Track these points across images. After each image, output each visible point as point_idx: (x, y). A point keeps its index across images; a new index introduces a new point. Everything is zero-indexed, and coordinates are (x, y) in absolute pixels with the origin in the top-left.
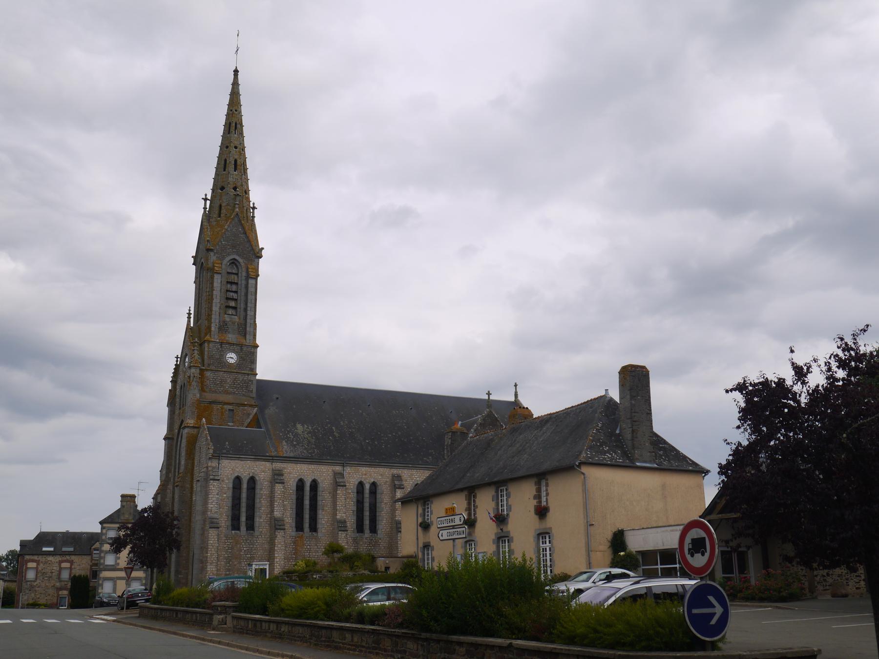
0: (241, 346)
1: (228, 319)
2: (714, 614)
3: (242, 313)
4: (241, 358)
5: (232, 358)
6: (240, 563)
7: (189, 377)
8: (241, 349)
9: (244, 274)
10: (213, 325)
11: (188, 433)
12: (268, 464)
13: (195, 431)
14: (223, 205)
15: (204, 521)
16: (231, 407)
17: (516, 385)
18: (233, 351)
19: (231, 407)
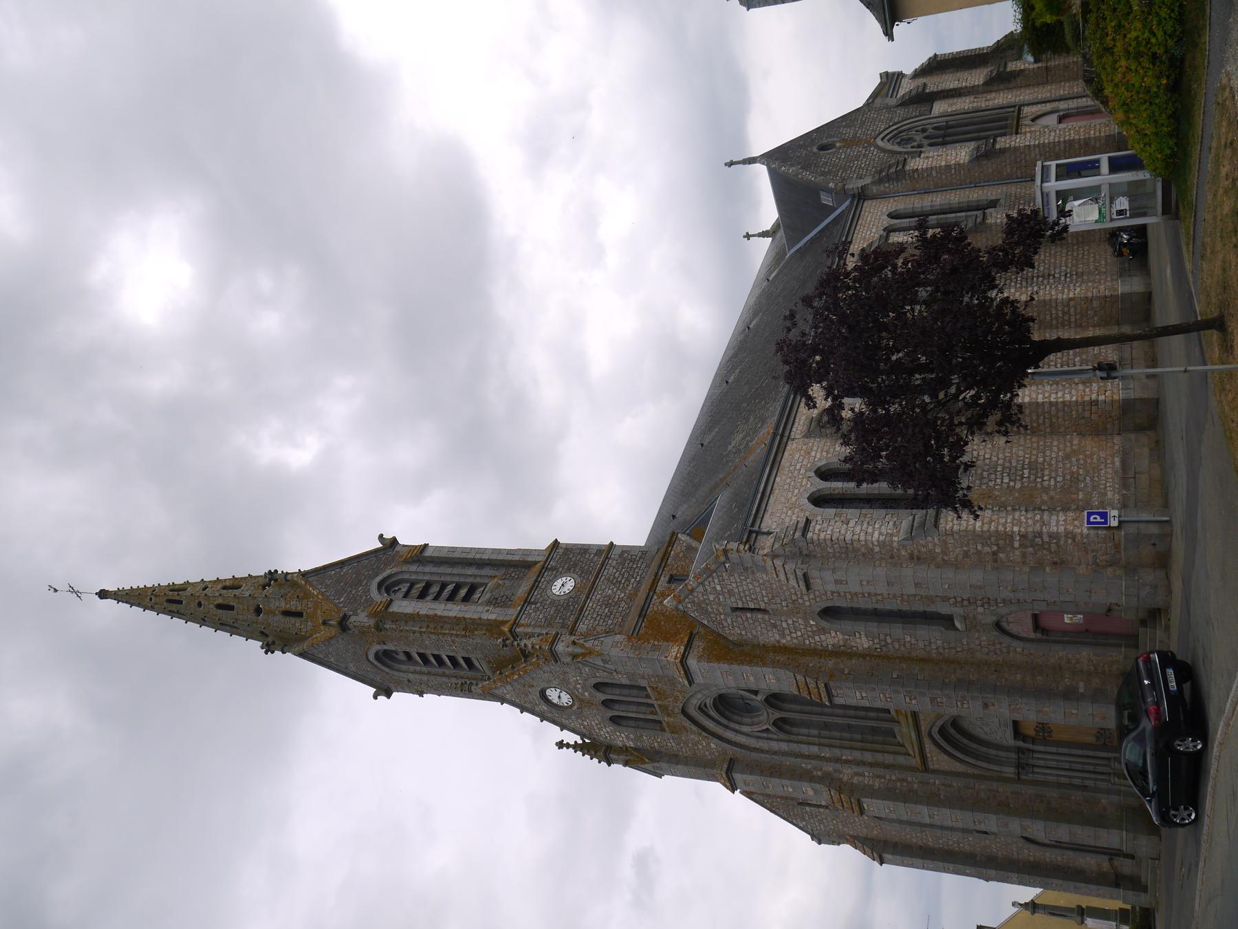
0: (545, 568)
1: (488, 596)
2: (1144, 729)
3: (487, 571)
4: (569, 570)
5: (563, 586)
6: (1046, 490)
7: (574, 656)
8: (552, 569)
9: (413, 568)
10: (485, 617)
11: (700, 659)
12: (791, 446)
13: (698, 644)
14: (283, 605)
15: (916, 559)
16: (663, 580)
17: (731, 164)
18: (551, 582)
19: (663, 580)
